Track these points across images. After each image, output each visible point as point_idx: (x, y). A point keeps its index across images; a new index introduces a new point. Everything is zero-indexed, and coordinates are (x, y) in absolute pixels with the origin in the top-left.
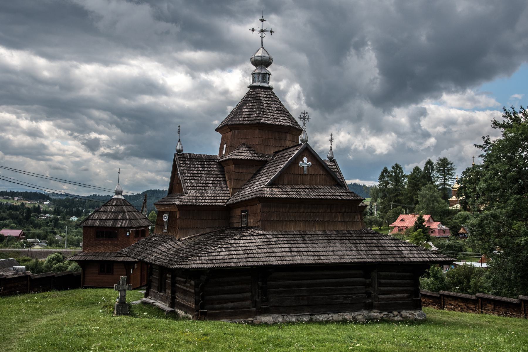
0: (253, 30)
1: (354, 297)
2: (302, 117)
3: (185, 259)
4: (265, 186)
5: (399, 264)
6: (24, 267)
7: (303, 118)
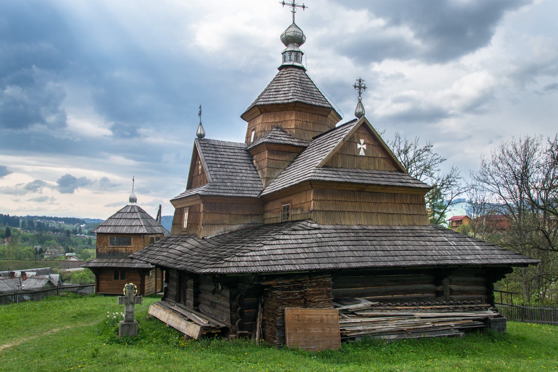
0: (304, 7)
2: (357, 85)
3: (218, 260)
4: (316, 167)
6: (35, 273)
7: (358, 87)
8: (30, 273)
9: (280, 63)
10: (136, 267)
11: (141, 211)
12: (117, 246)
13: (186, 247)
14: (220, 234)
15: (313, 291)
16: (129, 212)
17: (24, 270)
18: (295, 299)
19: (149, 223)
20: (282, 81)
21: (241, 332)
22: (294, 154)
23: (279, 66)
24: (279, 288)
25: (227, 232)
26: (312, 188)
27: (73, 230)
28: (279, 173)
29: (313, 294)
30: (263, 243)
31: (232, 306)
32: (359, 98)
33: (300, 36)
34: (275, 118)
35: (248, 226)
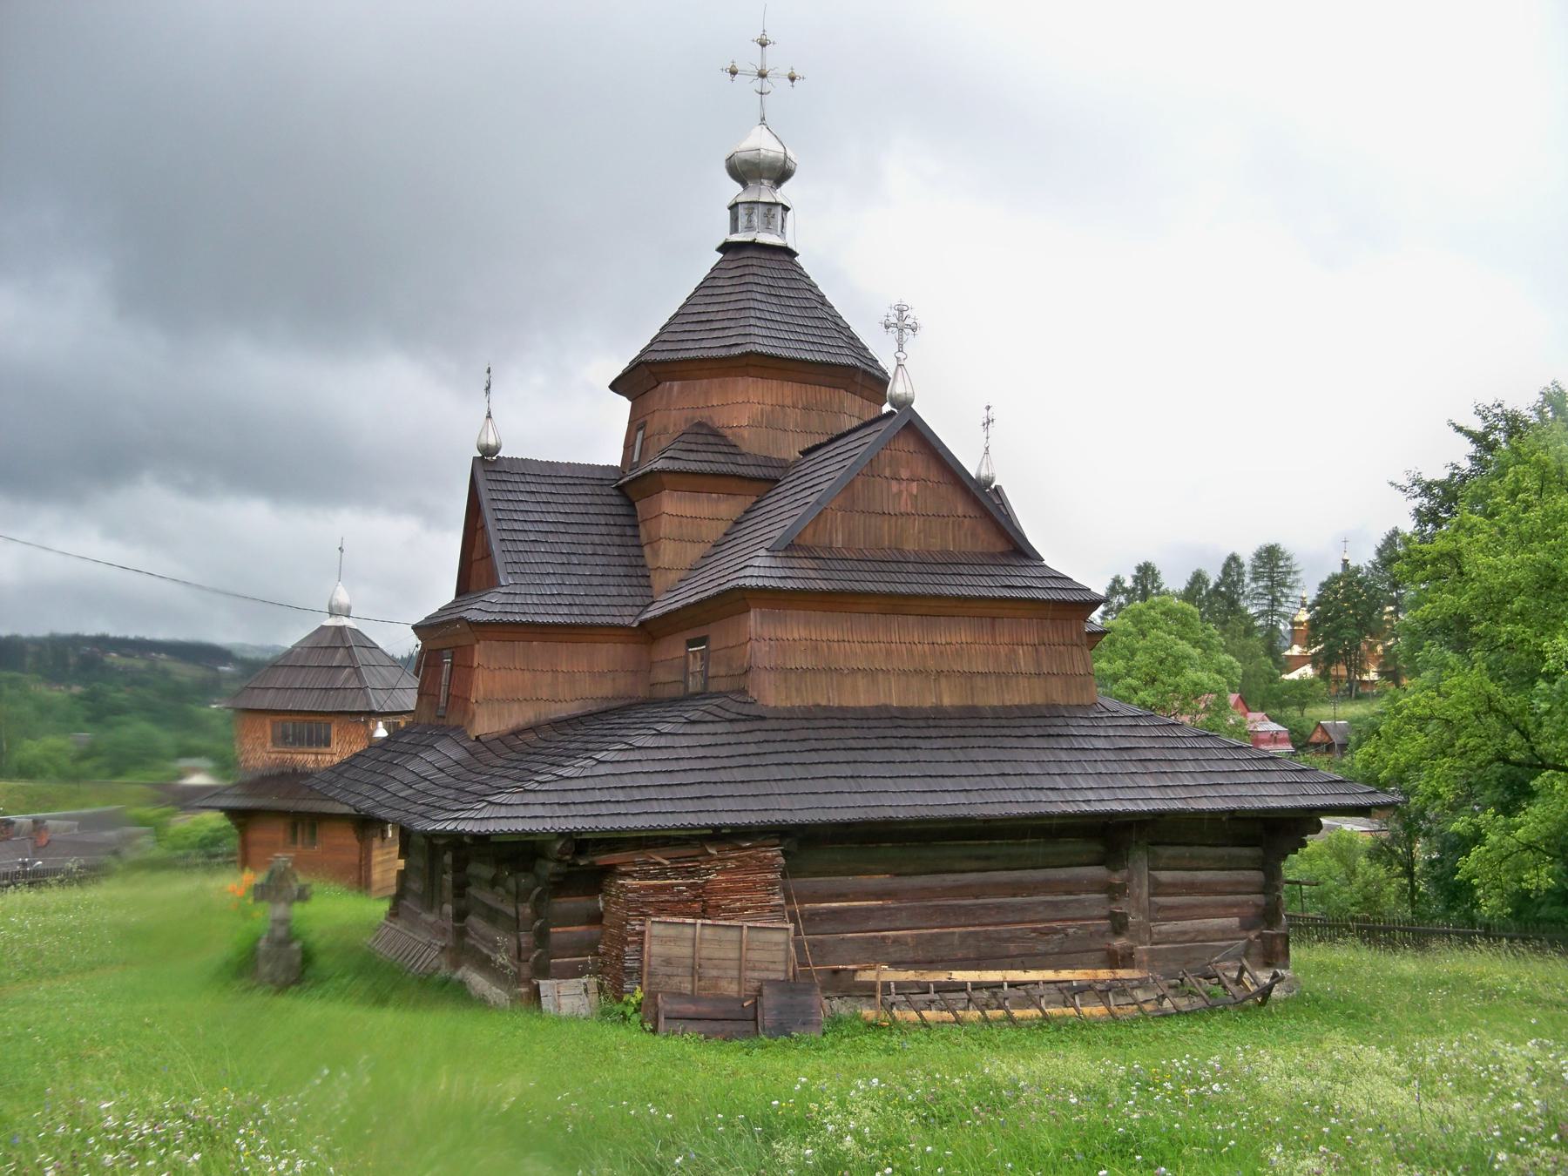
0: (733, 73)
1: (1071, 931)
5: (1224, 819)
9: (725, 235)
15: (727, 881)
18: (678, 902)
23: (720, 242)
24: (636, 871)
29: (726, 889)
30: (597, 757)
31: (520, 917)
32: (899, 355)
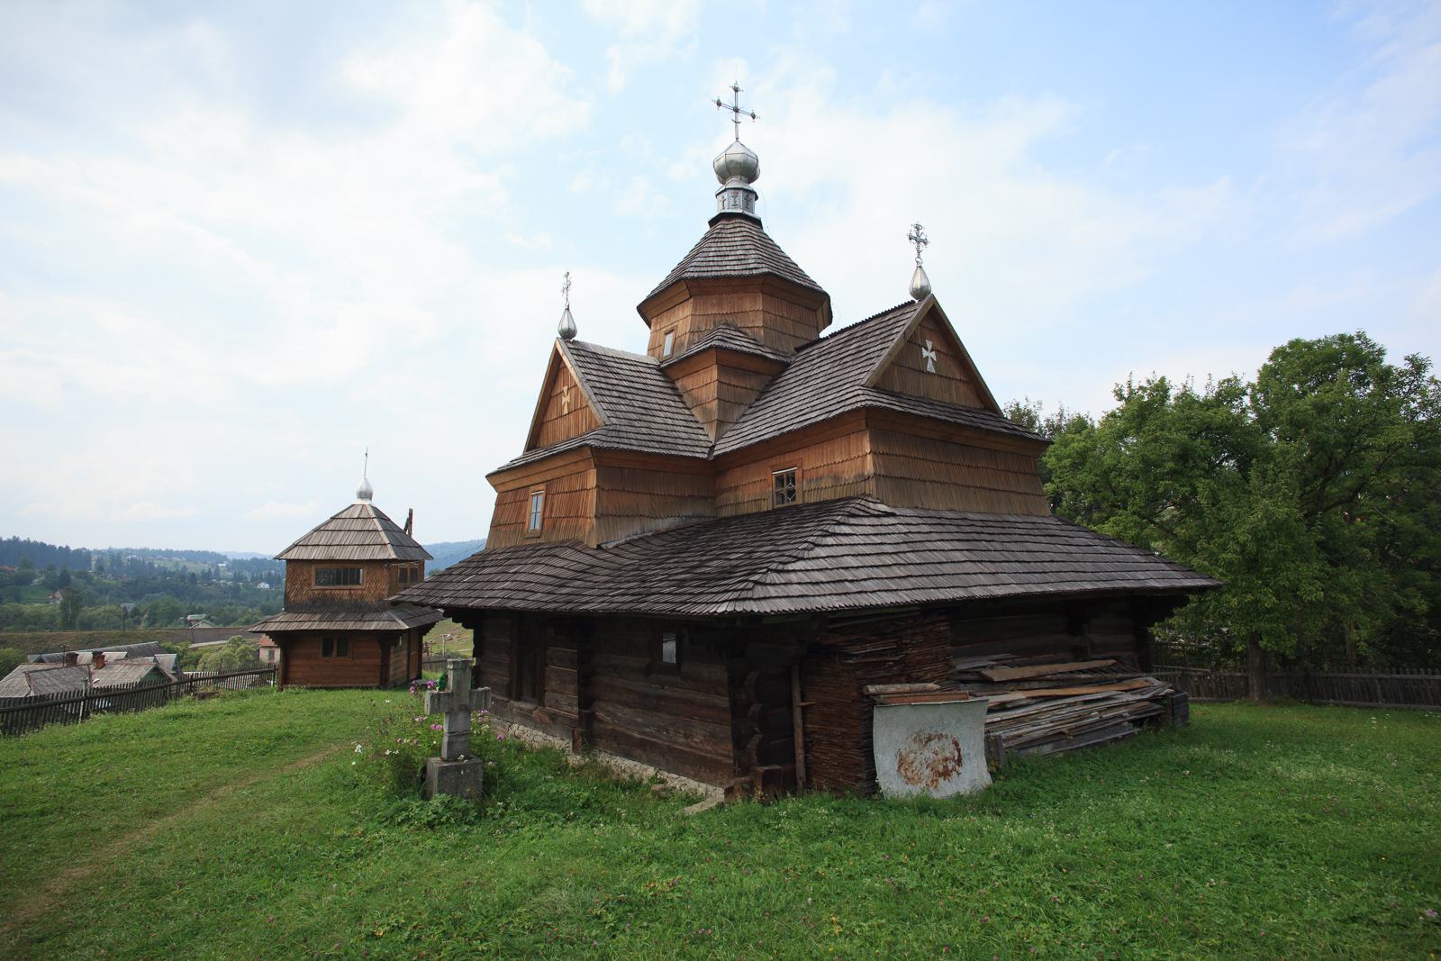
0: (754, 117)
8: (110, 655)
10: (372, 628)
11: (381, 516)
12: (332, 587)
13: (562, 568)
14: (636, 537)
16: (358, 518)
17: (98, 650)
19: (396, 538)
20: (726, 240)
21: (766, 768)
22: (765, 377)
25: (650, 534)
26: (867, 426)
27: (203, 572)
28: (741, 414)
32: (918, 259)
33: (753, 163)
34: (720, 304)
35: (688, 521)
